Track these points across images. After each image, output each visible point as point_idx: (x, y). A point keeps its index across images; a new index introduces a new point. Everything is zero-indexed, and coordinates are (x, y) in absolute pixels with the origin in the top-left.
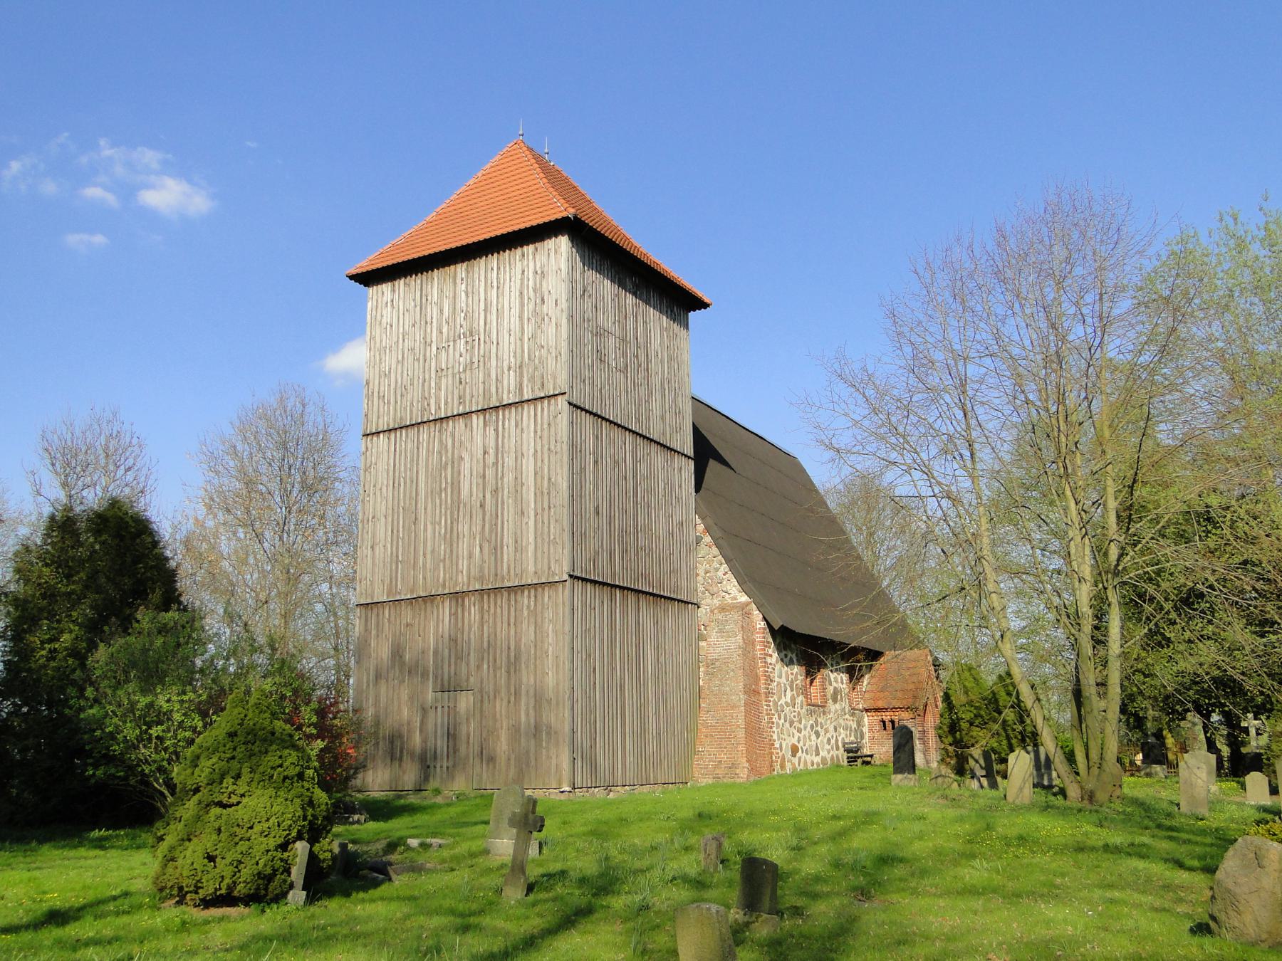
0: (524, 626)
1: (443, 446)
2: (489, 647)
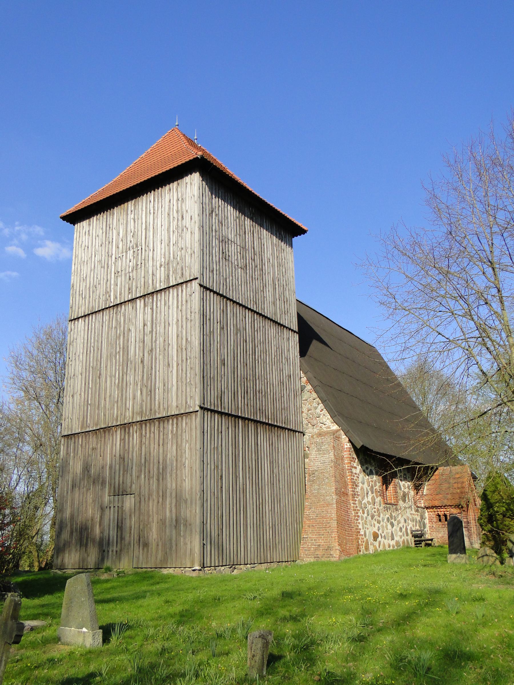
0: (169, 446)
1: (118, 323)
2: (145, 463)
